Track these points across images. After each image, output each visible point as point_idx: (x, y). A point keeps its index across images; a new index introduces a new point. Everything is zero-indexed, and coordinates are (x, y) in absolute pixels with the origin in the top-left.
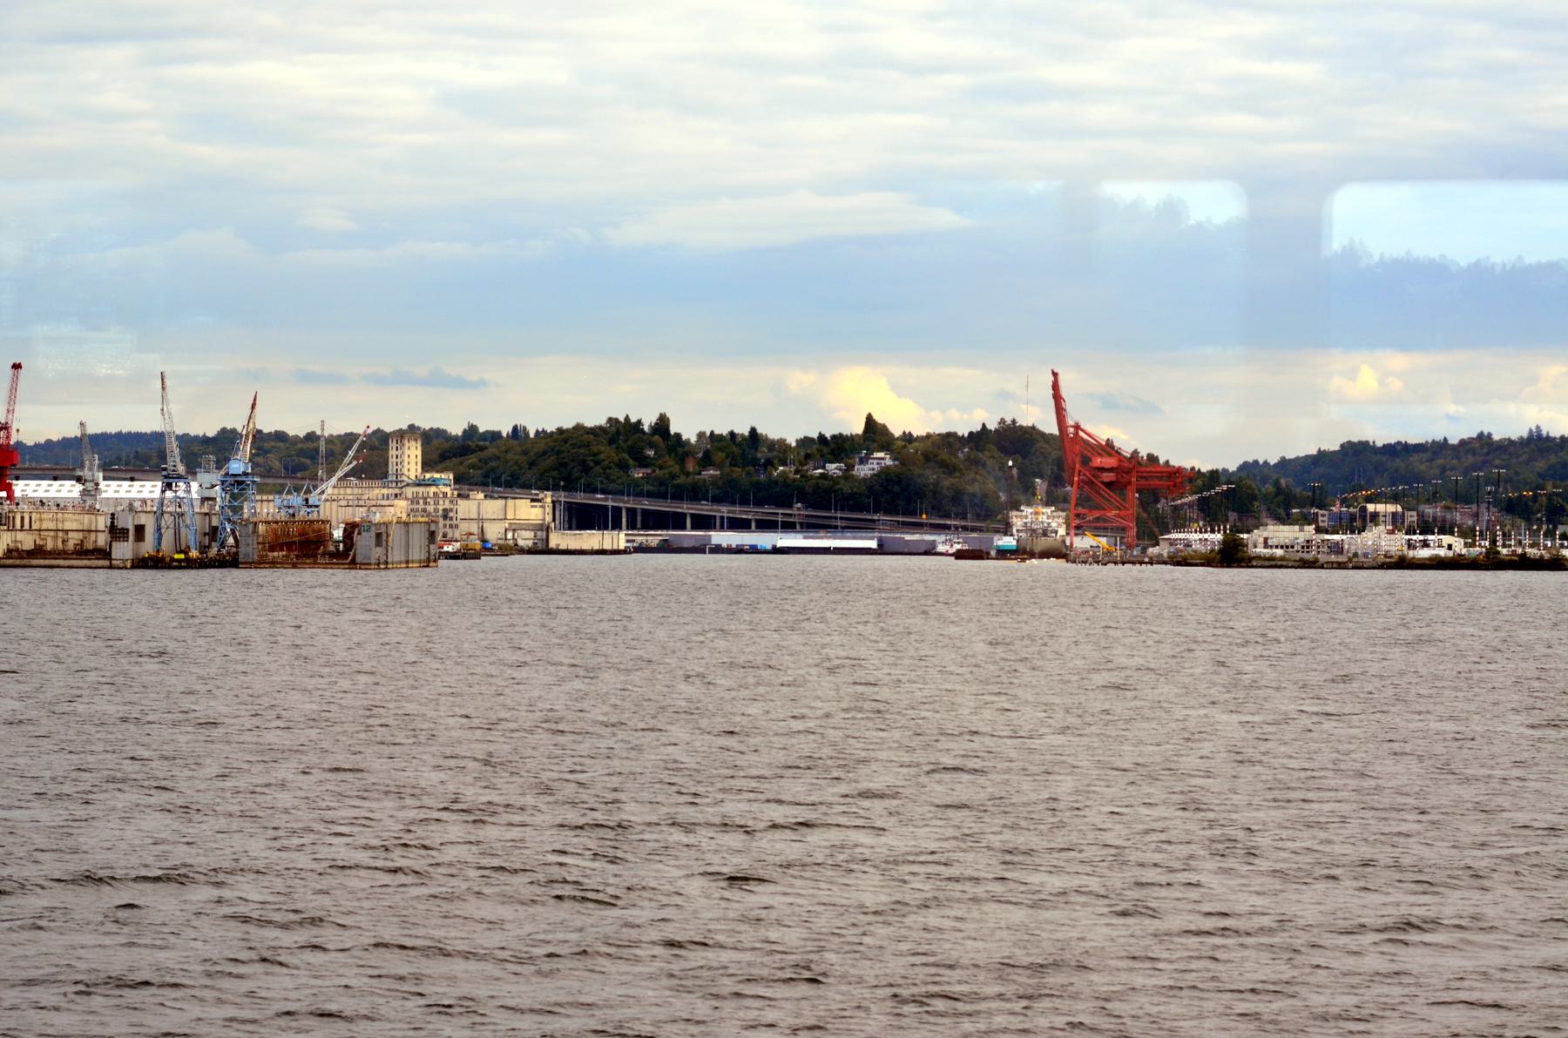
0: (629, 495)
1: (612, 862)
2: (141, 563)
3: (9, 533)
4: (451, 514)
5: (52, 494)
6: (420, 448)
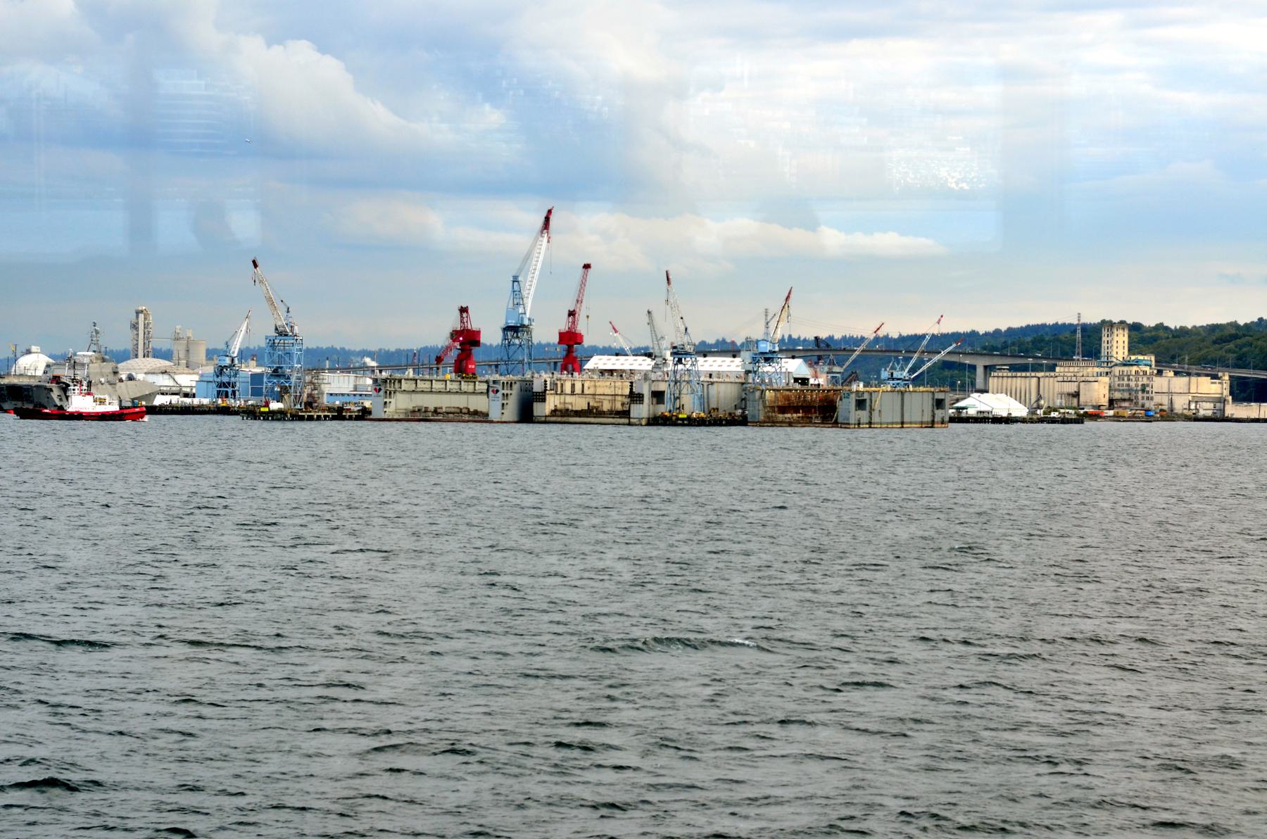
2: (655, 421)
3: (557, 397)
4: (1147, 389)
6: (1126, 336)
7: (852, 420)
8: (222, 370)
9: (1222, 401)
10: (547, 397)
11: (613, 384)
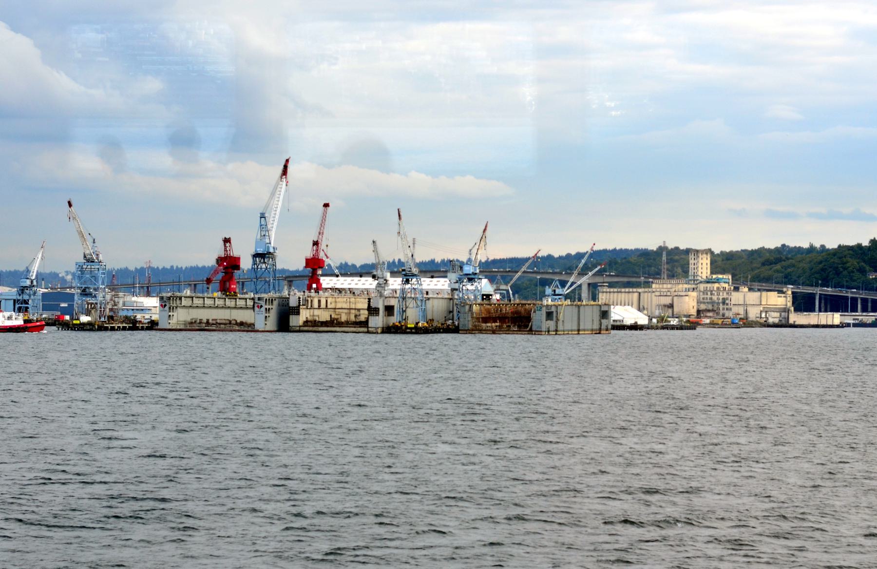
0: (862, 290)
1: (308, 557)
2: (389, 330)
3: (308, 311)
4: (727, 302)
5: (432, 287)
6: (709, 259)
7: (544, 329)
8: (23, 290)
9: (786, 310)
10: (301, 310)
11: (348, 300)
